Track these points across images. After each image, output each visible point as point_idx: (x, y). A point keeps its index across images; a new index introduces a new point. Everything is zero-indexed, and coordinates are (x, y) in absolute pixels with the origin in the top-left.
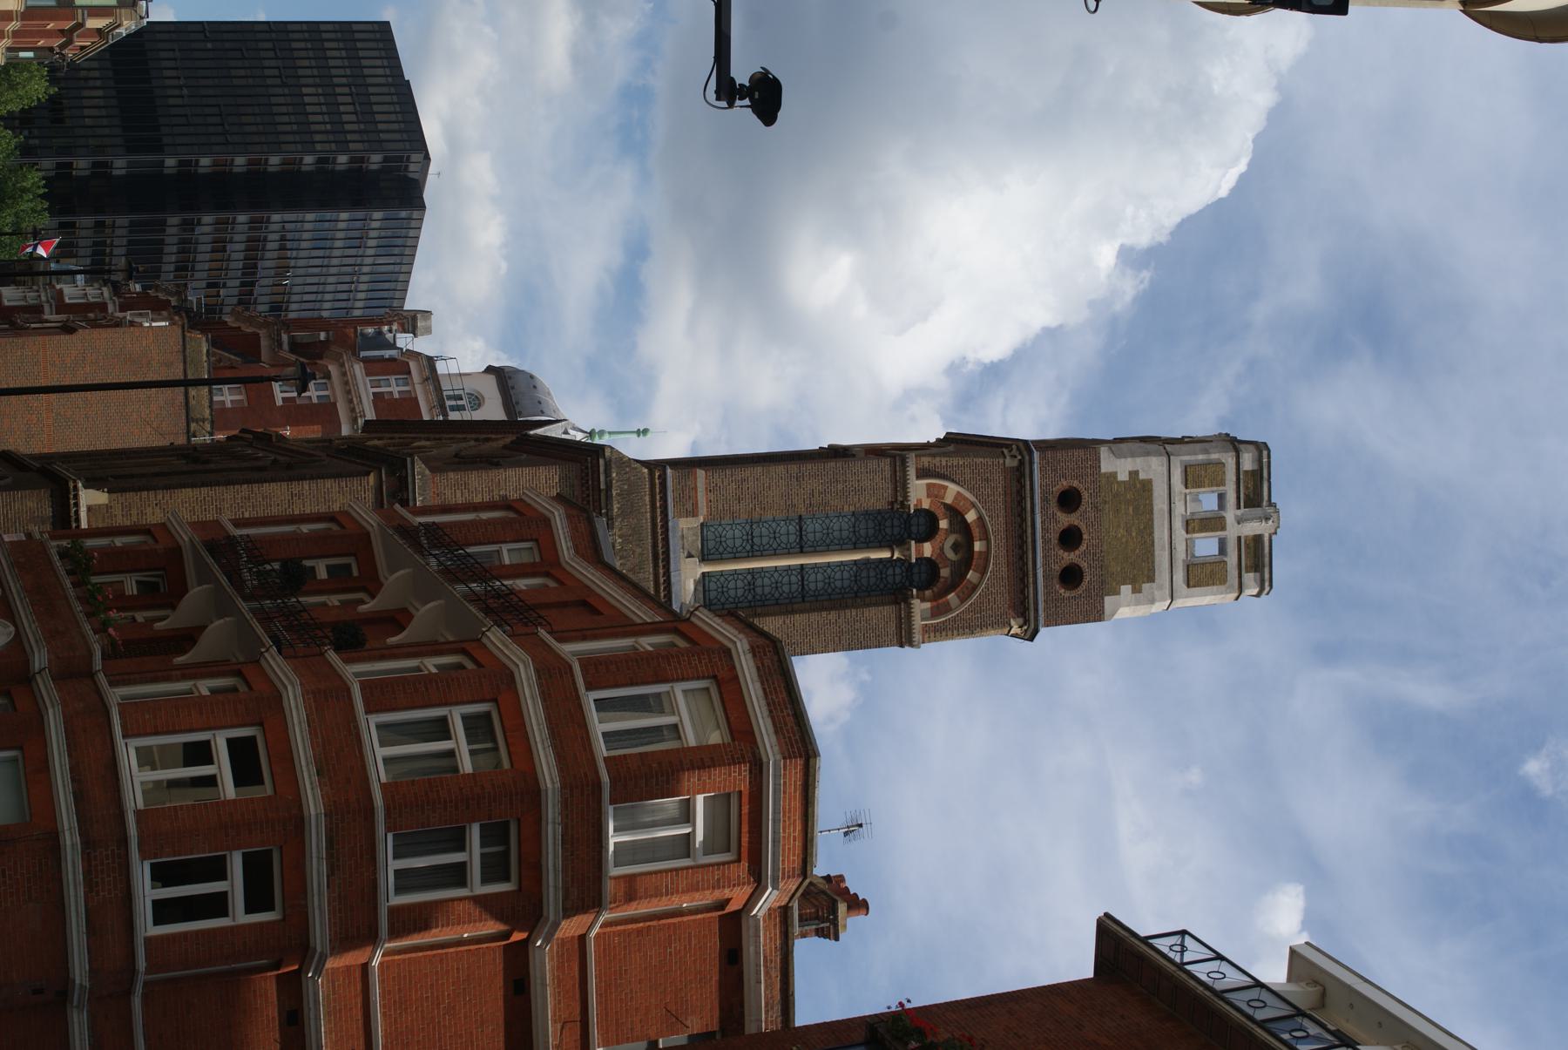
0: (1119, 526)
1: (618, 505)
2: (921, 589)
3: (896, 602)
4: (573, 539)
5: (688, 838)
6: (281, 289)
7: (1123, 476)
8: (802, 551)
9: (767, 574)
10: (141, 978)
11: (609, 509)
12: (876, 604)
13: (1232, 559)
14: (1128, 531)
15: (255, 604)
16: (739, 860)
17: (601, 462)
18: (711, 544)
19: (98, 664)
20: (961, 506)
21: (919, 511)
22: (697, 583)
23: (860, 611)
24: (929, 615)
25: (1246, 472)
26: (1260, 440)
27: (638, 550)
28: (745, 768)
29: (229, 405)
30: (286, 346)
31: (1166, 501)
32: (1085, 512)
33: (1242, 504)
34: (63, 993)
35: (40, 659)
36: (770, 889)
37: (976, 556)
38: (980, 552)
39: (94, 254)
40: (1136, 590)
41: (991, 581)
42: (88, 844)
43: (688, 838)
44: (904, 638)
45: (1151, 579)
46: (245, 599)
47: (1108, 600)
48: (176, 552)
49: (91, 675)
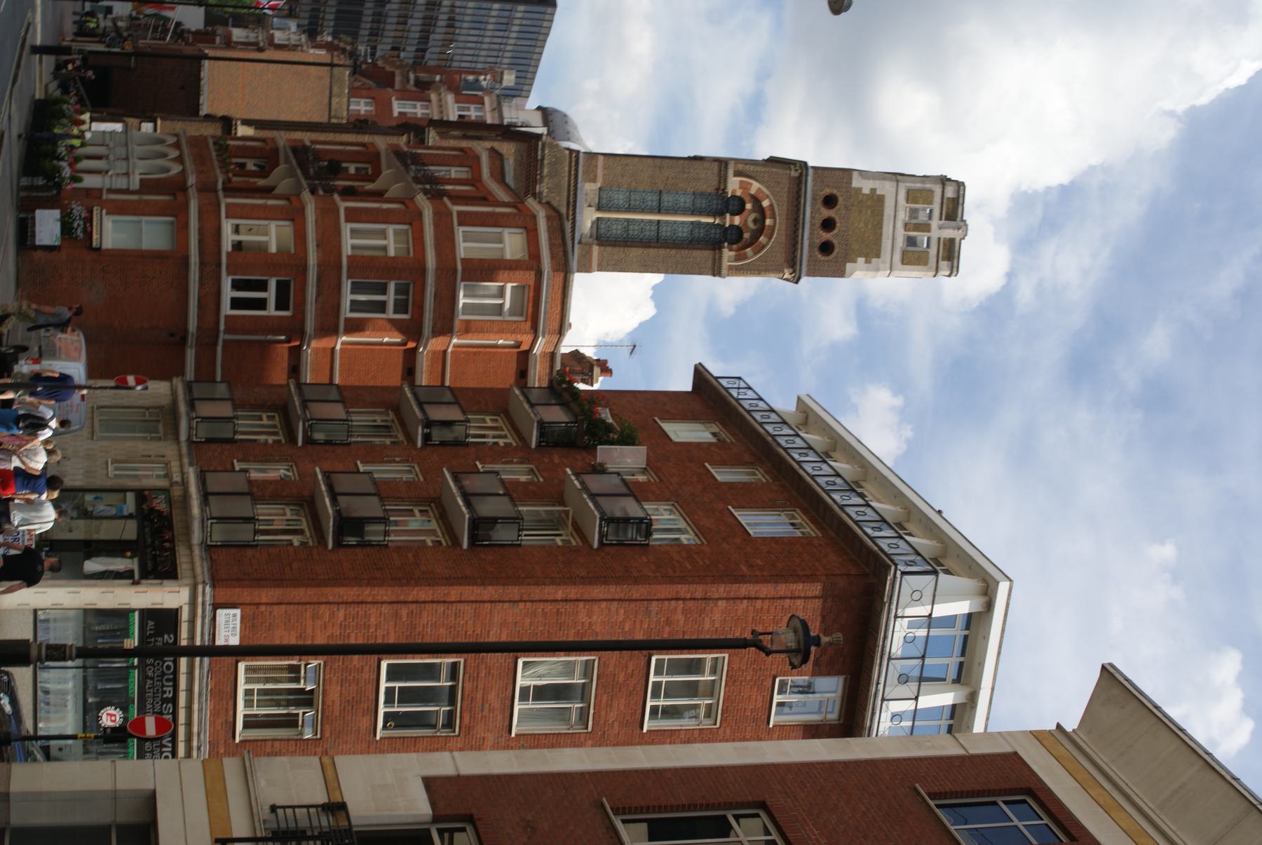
0: (860, 220)
2: (731, 243)
3: (714, 249)
4: (491, 168)
5: (501, 306)
6: (445, 57)
7: (866, 191)
8: (659, 212)
10: (222, 337)
11: (542, 172)
12: (701, 249)
13: (933, 251)
14: (866, 224)
15: (309, 182)
16: (526, 321)
17: (540, 143)
18: (604, 201)
19: (220, 186)
20: (760, 196)
21: (734, 197)
22: (593, 223)
23: (690, 251)
24: (733, 259)
25: (948, 198)
26: (960, 180)
27: (558, 198)
28: (533, 273)
29: (363, 112)
30: (412, 82)
31: (893, 210)
32: (839, 209)
33: (943, 218)
34: (184, 339)
35: (192, 180)
36: (540, 338)
37: (766, 228)
38: (769, 226)
39: (311, 17)
40: (868, 262)
41: (774, 243)
42: (202, 264)
43: (501, 306)
44: (716, 271)
45: (878, 256)
46: (306, 178)
47: (849, 266)
48: (276, 150)
49: (216, 191)
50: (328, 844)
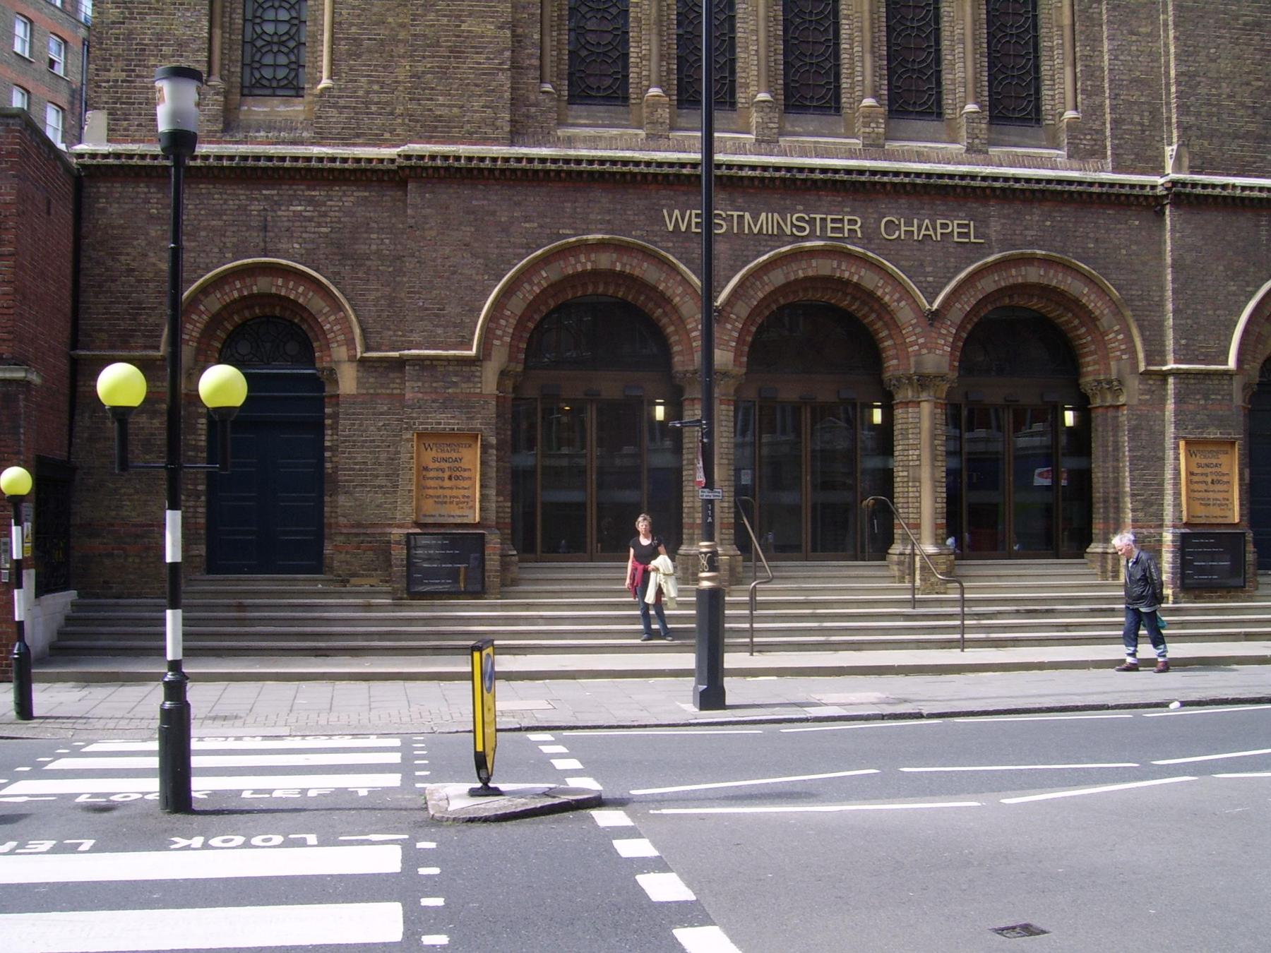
1: (648, 110)
9: (257, 58)
50: (63, 2)
